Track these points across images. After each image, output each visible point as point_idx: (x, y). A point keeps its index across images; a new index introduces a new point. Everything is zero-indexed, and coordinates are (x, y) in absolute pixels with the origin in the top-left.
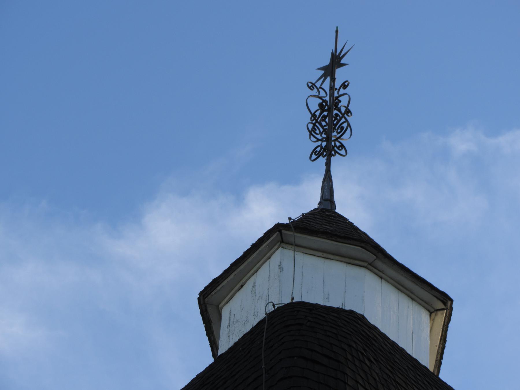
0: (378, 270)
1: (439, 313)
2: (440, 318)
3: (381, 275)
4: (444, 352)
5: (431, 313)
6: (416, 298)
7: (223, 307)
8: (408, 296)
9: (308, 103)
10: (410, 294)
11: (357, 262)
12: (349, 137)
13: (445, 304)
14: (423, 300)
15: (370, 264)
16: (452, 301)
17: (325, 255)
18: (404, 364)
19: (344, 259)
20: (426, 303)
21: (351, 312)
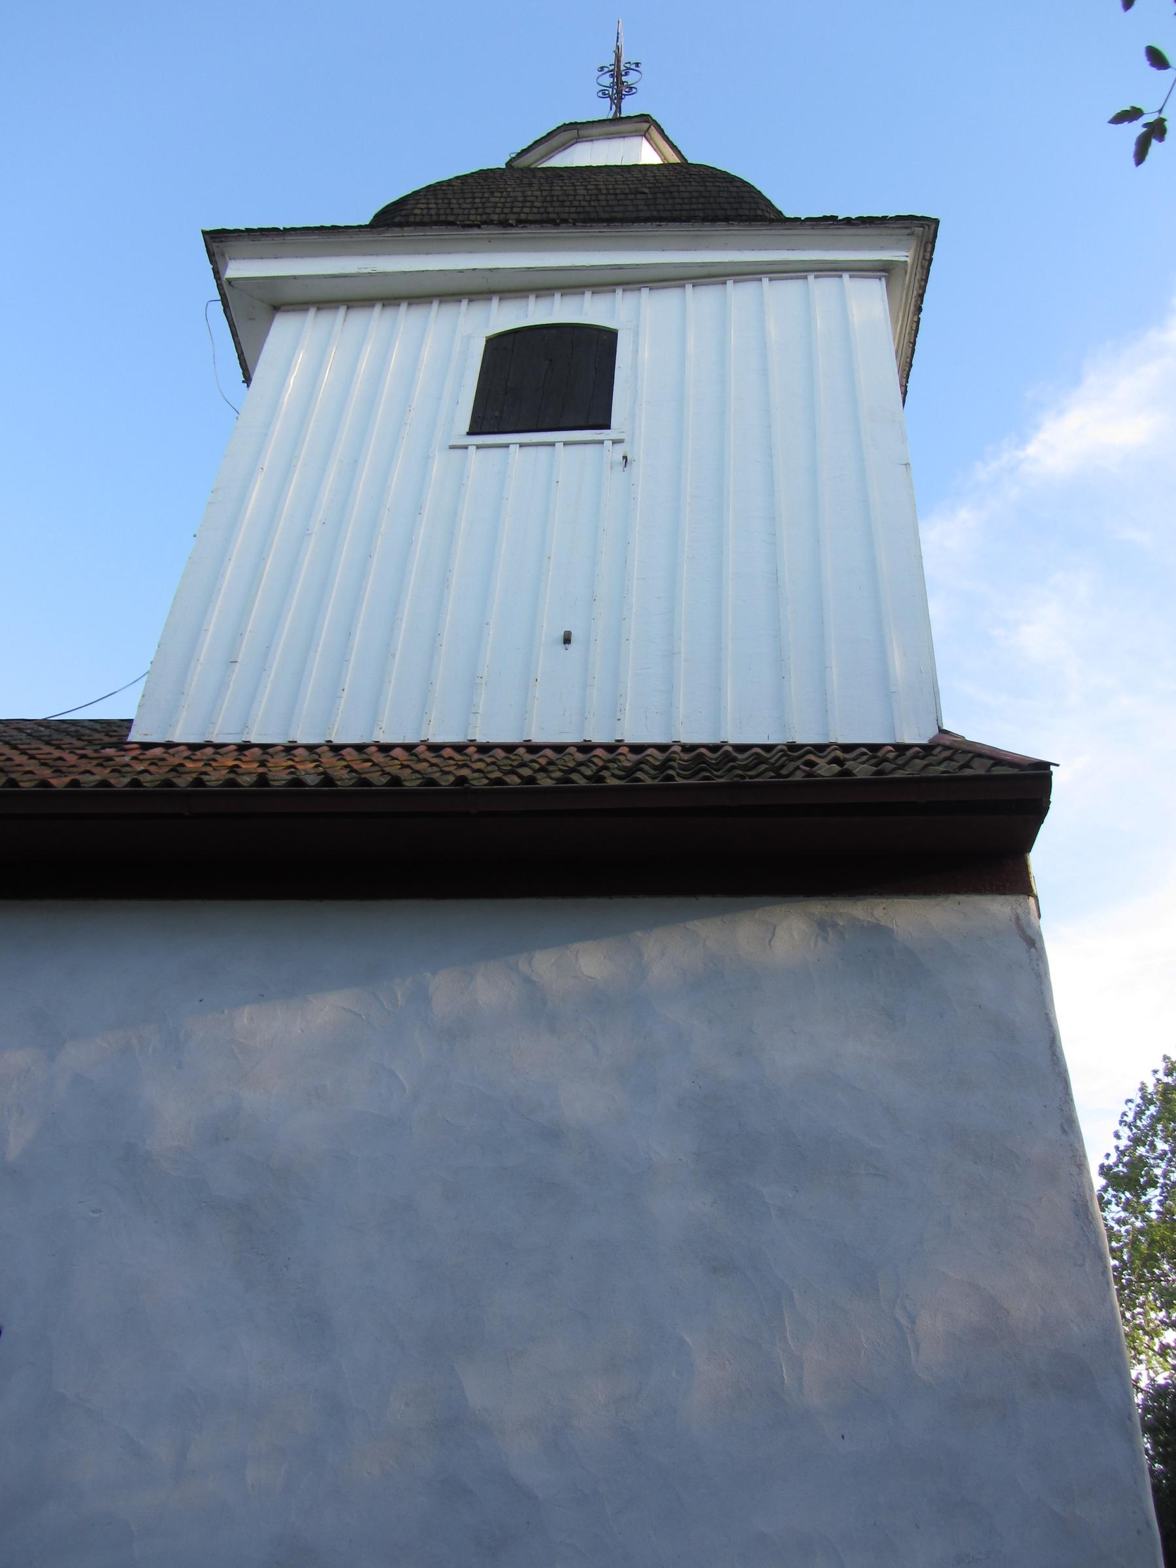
0: (586, 137)
1: (650, 130)
2: (654, 132)
3: (590, 139)
4: (259, 228)
5: (644, 136)
6: (627, 135)
7: (699, 285)
8: (620, 137)
9: (635, 72)
10: (620, 135)
11: (569, 144)
12: (639, 73)
13: (648, 122)
14: (632, 132)
15: (579, 138)
16: (648, 115)
17: (548, 157)
18: (361, 269)
19: (560, 149)
20: (636, 132)
21: (1122, 123)
